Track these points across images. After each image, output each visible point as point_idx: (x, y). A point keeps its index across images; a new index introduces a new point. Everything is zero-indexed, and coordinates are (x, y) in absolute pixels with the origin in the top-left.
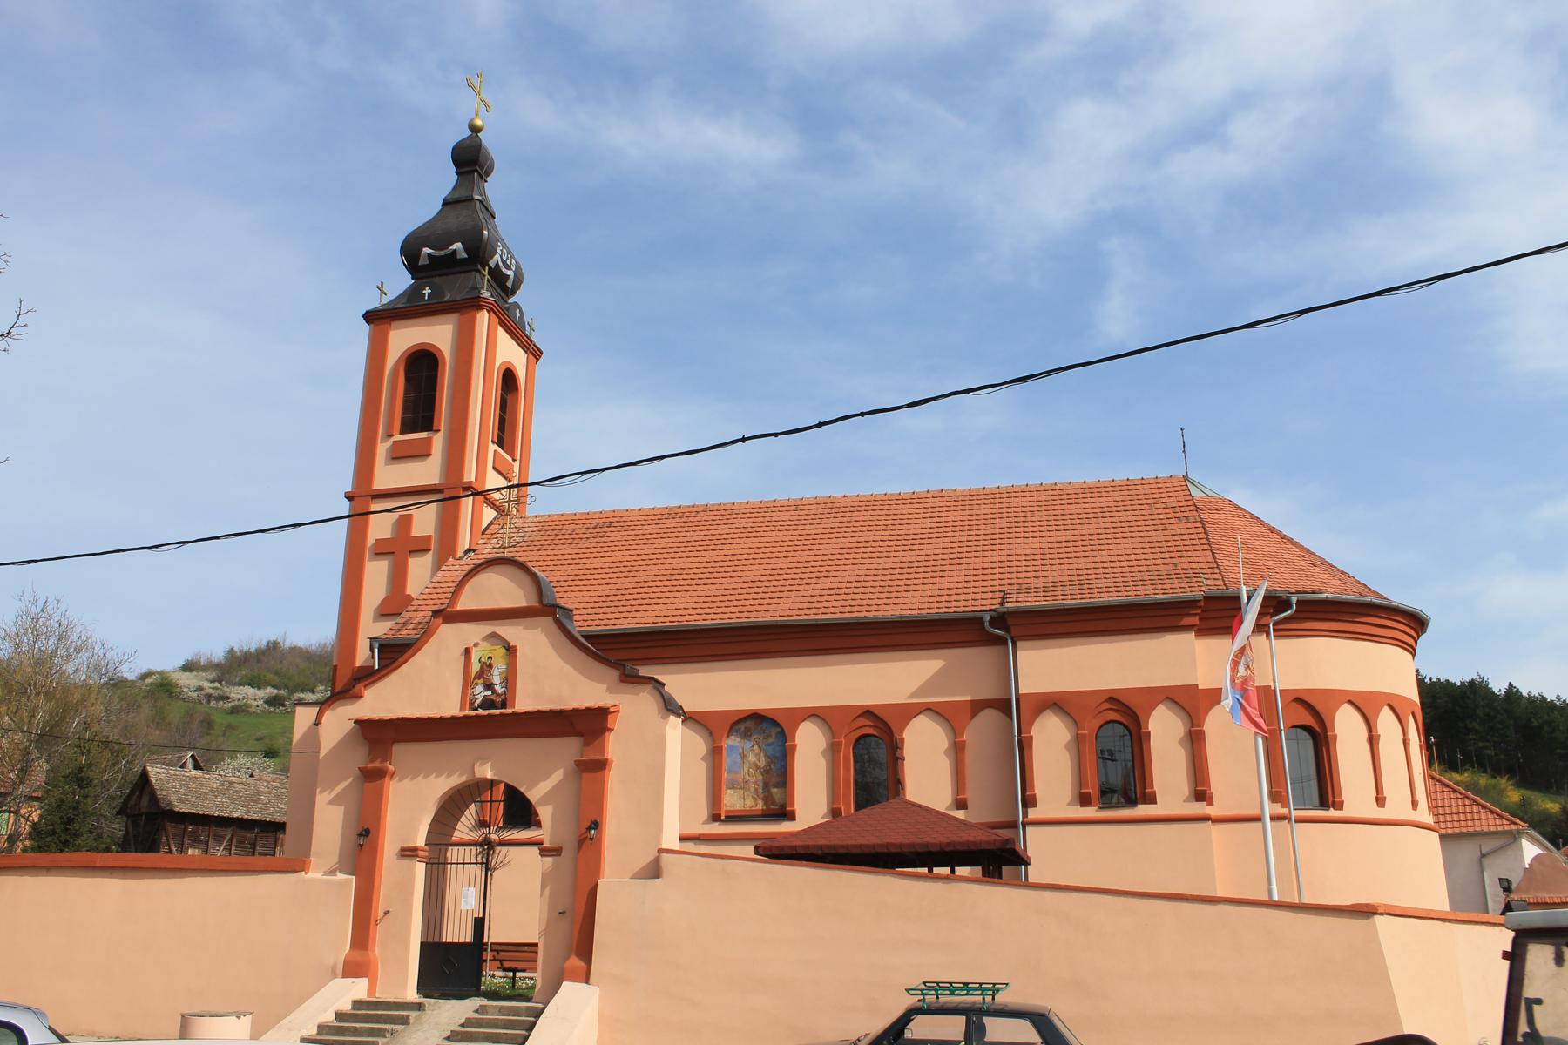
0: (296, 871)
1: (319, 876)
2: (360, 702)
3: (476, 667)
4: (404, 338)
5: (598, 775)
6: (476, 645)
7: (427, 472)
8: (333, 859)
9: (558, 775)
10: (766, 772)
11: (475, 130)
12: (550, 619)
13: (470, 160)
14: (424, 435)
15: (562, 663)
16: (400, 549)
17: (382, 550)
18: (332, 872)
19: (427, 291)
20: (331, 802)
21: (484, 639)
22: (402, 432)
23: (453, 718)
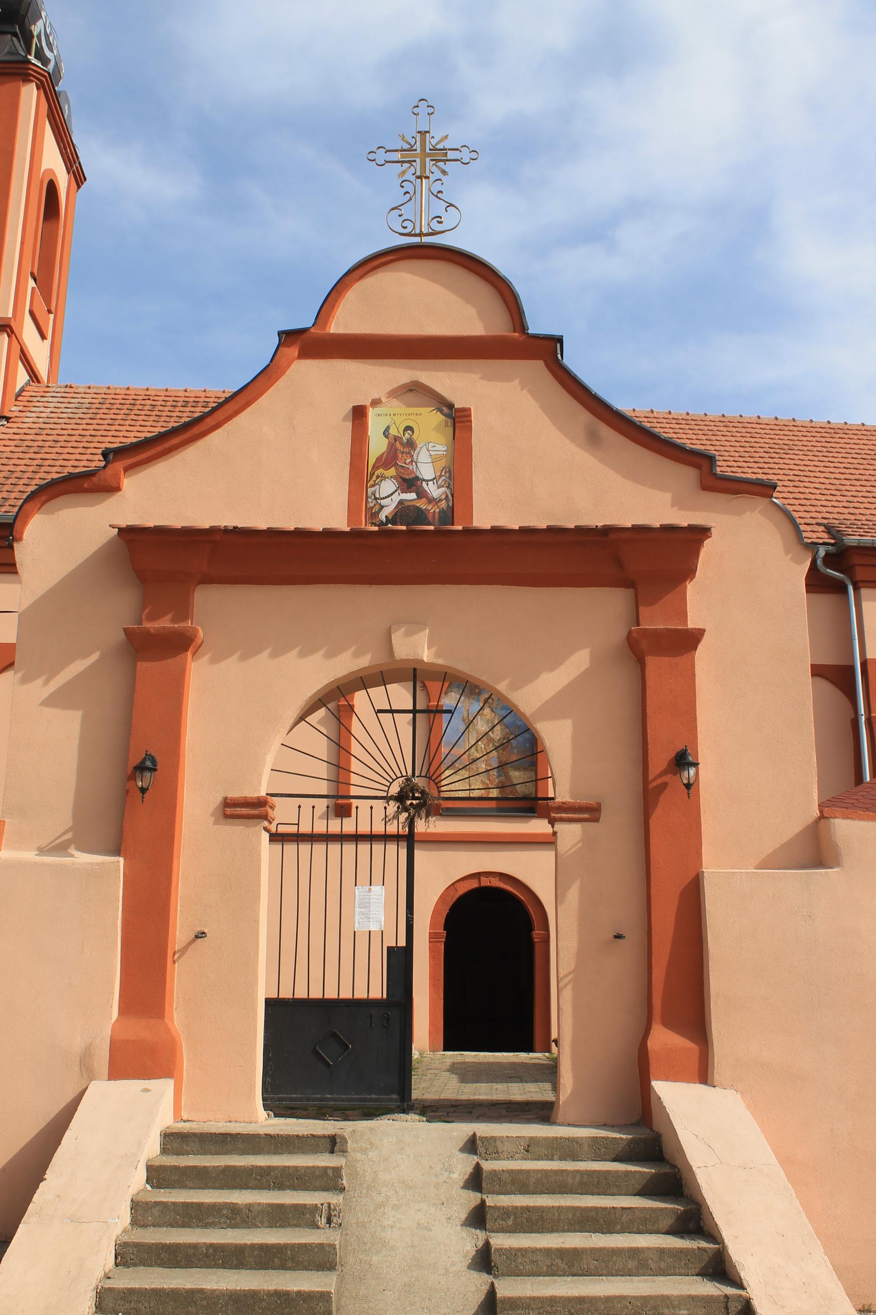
1: (30, 856)
2: (113, 500)
3: (377, 446)
5: (684, 658)
6: (376, 403)
8: (60, 817)
9: (579, 662)
10: (502, 746)
12: (540, 364)
18: (60, 848)
20: (50, 702)
21: (395, 393)
23: (329, 534)
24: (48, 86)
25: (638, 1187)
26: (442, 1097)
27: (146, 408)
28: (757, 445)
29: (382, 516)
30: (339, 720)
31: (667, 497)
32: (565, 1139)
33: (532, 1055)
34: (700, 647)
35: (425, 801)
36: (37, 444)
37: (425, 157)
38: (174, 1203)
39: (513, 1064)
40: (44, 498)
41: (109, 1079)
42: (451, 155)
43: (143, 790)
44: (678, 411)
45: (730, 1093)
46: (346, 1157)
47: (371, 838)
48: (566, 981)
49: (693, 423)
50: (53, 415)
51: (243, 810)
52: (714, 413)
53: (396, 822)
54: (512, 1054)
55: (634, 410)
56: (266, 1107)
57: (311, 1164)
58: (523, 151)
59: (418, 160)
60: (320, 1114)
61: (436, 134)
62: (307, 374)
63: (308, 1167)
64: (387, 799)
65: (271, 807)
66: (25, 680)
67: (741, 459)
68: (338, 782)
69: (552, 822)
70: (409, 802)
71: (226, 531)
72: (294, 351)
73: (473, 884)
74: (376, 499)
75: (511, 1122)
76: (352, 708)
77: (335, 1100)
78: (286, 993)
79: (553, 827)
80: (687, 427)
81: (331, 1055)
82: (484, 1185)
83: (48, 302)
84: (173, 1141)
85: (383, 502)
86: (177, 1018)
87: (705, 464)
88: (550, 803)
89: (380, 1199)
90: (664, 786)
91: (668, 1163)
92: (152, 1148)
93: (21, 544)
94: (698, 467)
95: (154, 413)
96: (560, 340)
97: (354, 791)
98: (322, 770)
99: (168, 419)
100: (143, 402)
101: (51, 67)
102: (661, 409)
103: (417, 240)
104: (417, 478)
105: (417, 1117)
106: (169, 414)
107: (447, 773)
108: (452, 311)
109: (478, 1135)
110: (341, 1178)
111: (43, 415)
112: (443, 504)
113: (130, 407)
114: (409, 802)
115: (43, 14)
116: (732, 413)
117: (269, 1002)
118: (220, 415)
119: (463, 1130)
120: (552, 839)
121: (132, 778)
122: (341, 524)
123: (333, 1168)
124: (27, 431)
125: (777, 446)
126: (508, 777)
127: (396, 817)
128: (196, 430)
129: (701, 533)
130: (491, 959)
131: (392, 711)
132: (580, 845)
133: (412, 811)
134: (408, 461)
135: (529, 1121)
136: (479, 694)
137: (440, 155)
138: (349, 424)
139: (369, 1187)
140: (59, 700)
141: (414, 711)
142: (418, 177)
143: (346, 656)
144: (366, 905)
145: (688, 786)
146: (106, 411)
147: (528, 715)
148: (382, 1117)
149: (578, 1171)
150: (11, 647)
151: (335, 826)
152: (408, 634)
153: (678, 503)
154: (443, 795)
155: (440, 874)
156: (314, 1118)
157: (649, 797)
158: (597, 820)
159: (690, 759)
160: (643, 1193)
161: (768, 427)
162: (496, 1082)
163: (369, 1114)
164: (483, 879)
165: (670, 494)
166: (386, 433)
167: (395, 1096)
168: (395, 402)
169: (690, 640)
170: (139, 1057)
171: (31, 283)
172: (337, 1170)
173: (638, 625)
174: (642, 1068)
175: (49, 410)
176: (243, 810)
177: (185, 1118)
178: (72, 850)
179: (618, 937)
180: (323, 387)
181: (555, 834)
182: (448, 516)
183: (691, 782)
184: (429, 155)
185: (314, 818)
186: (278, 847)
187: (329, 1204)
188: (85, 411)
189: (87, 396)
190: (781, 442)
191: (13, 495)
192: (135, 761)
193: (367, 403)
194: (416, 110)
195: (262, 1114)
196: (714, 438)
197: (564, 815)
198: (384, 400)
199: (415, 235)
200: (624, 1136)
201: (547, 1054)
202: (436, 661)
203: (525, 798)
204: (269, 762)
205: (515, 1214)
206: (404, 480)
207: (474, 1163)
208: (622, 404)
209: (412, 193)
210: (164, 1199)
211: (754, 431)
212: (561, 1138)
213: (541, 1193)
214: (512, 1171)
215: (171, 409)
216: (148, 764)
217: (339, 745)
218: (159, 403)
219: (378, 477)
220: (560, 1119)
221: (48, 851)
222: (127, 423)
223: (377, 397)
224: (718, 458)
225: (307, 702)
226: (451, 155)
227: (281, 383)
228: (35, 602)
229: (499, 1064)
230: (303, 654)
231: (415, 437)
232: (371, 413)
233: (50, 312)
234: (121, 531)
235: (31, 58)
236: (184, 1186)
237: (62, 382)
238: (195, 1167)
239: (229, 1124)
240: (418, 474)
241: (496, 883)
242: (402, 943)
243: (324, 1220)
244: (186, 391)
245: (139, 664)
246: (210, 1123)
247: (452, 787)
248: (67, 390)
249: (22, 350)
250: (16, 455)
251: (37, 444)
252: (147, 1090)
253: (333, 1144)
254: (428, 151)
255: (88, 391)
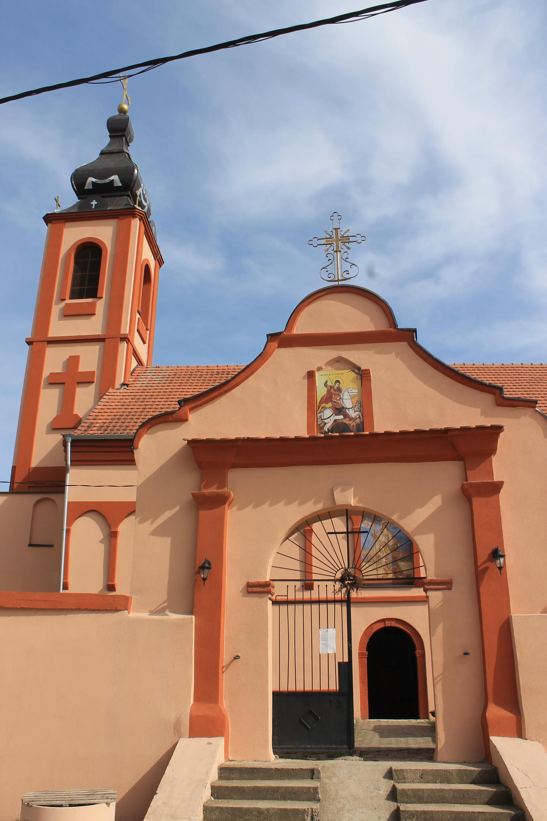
0: (117, 610)
1: (145, 615)
2: (185, 426)
3: (321, 392)
4: (74, 234)
5: (494, 498)
7: (93, 326)
8: (161, 595)
9: (436, 502)
10: (394, 550)
11: (122, 111)
12: (405, 344)
13: (119, 129)
14: (90, 300)
15: (425, 387)
16: (69, 380)
17: (54, 381)
18: (161, 611)
19: (94, 203)
20: (154, 533)
22: (71, 298)
23: (298, 439)
24: (145, 219)
25: (487, 800)
26: (371, 746)
27: (198, 376)
28: (523, 379)
29: (326, 428)
30: (305, 536)
31: (479, 410)
32: (442, 770)
33: (418, 721)
34: (502, 491)
35: (356, 582)
36: (142, 397)
37: (338, 241)
38: (227, 808)
39: (409, 726)
40: (149, 426)
41: (190, 737)
42: (351, 239)
43: (204, 579)
44: (478, 363)
45: (536, 743)
46: (320, 781)
47: (327, 602)
48: (438, 679)
49: (487, 369)
50: (150, 382)
51: (258, 589)
52: (498, 363)
53: (340, 593)
54: (407, 720)
55: (454, 364)
56: (275, 753)
57: (301, 786)
58: (388, 234)
59: (335, 243)
60: (304, 757)
61: (343, 229)
62: (282, 355)
63: (299, 787)
64: (335, 581)
65: (273, 587)
66: (142, 521)
67: (515, 387)
68: (305, 572)
69: (426, 591)
70: (347, 582)
71: (244, 440)
72: (275, 344)
73: (382, 625)
74: (322, 419)
75: (411, 761)
76: (312, 530)
77: (312, 748)
78: (284, 688)
79: (426, 593)
80: (484, 371)
81: (309, 723)
82: (398, 798)
83: (146, 325)
84: (225, 772)
85: (326, 421)
86: (225, 703)
87: (497, 391)
88: (424, 580)
89: (340, 806)
90: (487, 568)
91: (503, 785)
92: (214, 776)
93: (138, 450)
94: (494, 394)
95: (202, 379)
96: (415, 331)
97: (314, 577)
98: (297, 565)
99: (209, 382)
100: (196, 373)
101: (146, 209)
102: (469, 363)
103: (336, 283)
104: (343, 407)
105: (358, 758)
106: (209, 379)
107: (364, 564)
108: (360, 320)
109: (393, 768)
110: (318, 793)
111: (145, 382)
112: (358, 421)
113: (189, 376)
114: (347, 582)
115: (142, 185)
116: (507, 363)
117: (276, 695)
118: (238, 379)
119: (385, 765)
120: (427, 600)
121: (198, 573)
122: (304, 433)
123: (313, 788)
124: (137, 391)
125: (533, 379)
126: (398, 566)
127: (340, 590)
128: (226, 388)
129: (497, 429)
130: (393, 667)
131: (335, 533)
132: (442, 603)
133: (349, 587)
134: (338, 399)
135: (421, 760)
136: (380, 521)
137: (346, 240)
138: (306, 381)
139: (333, 799)
140: (158, 532)
141: (347, 533)
142: (335, 252)
143: (310, 503)
144: (325, 639)
145: (500, 568)
146: (177, 379)
147: (409, 532)
148: (339, 758)
149: (451, 790)
150: (133, 503)
151: (307, 595)
152: (343, 491)
153: (484, 414)
154: (365, 577)
155: (365, 619)
156: (301, 759)
157: (479, 575)
158: (450, 589)
159: (500, 553)
160: (490, 803)
161: (528, 369)
162: (400, 737)
163: (331, 757)
164: (387, 622)
165: (480, 409)
166: (326, 385)
167: (345, 746)
168: (330, 368)
169: (497, 487)
170: (206, 725)
171: (138, 316)
172: (315, 789)
173: (467, 481)
174: (483, 730)
175: (148, 380)
176: (258, 589)
177: (230, 759)
178: (167, 612)
179: (466, 654)
180: (291, 362)
181: (427, 597)
182: (361, 427)
183: (502, 566)
184: (340, 240)
185: (293, 591)
186: (277, 607)
187: (312, 809)
188: (166, 379)
189: (167, 371)
190: (535, 377)
191: (131, 424)
192: (199, 564)
193: (315, 369)
194: (332, 218)
195: (272, 757)
196: (499, 377)
197: (432, 587)
198: (323, 367)
199: (335, 281)
200: (476, 769)
201: (427, 720)
202: (358, 505)
203: (408, 578)
204: (270, 563)
205: (417, 815)
206: (336, 409)
207: (392, 785)
208: (448, 362)
209: (332, 260)
210: (221, 806)
211: (520, 371)
212: (440, 770)
213: (431, 802)
214: (414, 789)
215: (211, 376)
216: (207, 565)
217: (305, 551)
218: (204, 373)
219: (322, 408)
220: (439, 759)
221: (155, 612)
222: (188, 384)
223: (320, 366)
224: (505, 390)
225: (290, 529)
226: (351, 239)
227: (269, 361)
228: (145, 481)
229: (400, 726)
230: (286, 504)
231: (341, 386)
232: (317, 374)
233: (147, 330)
234: (190, 442)
235: (137, 206)
236: (231, 798)
237: (154, 365)
238: (237, 787)
239: (255, 762)
240: (344, 405)
241: (394, 624)
242: (346, 660)
243: (309, 818)
244: (218, 366)
245: (200, 511)
246: (244, 762)
247: (368, 574)
248: (157, 369)
249: (134, 350)
250: (132, 404)
251: (142, 397)
252: (210, 743)
253: (312, 774)
254: (339, 238)
255: (168, 369)
